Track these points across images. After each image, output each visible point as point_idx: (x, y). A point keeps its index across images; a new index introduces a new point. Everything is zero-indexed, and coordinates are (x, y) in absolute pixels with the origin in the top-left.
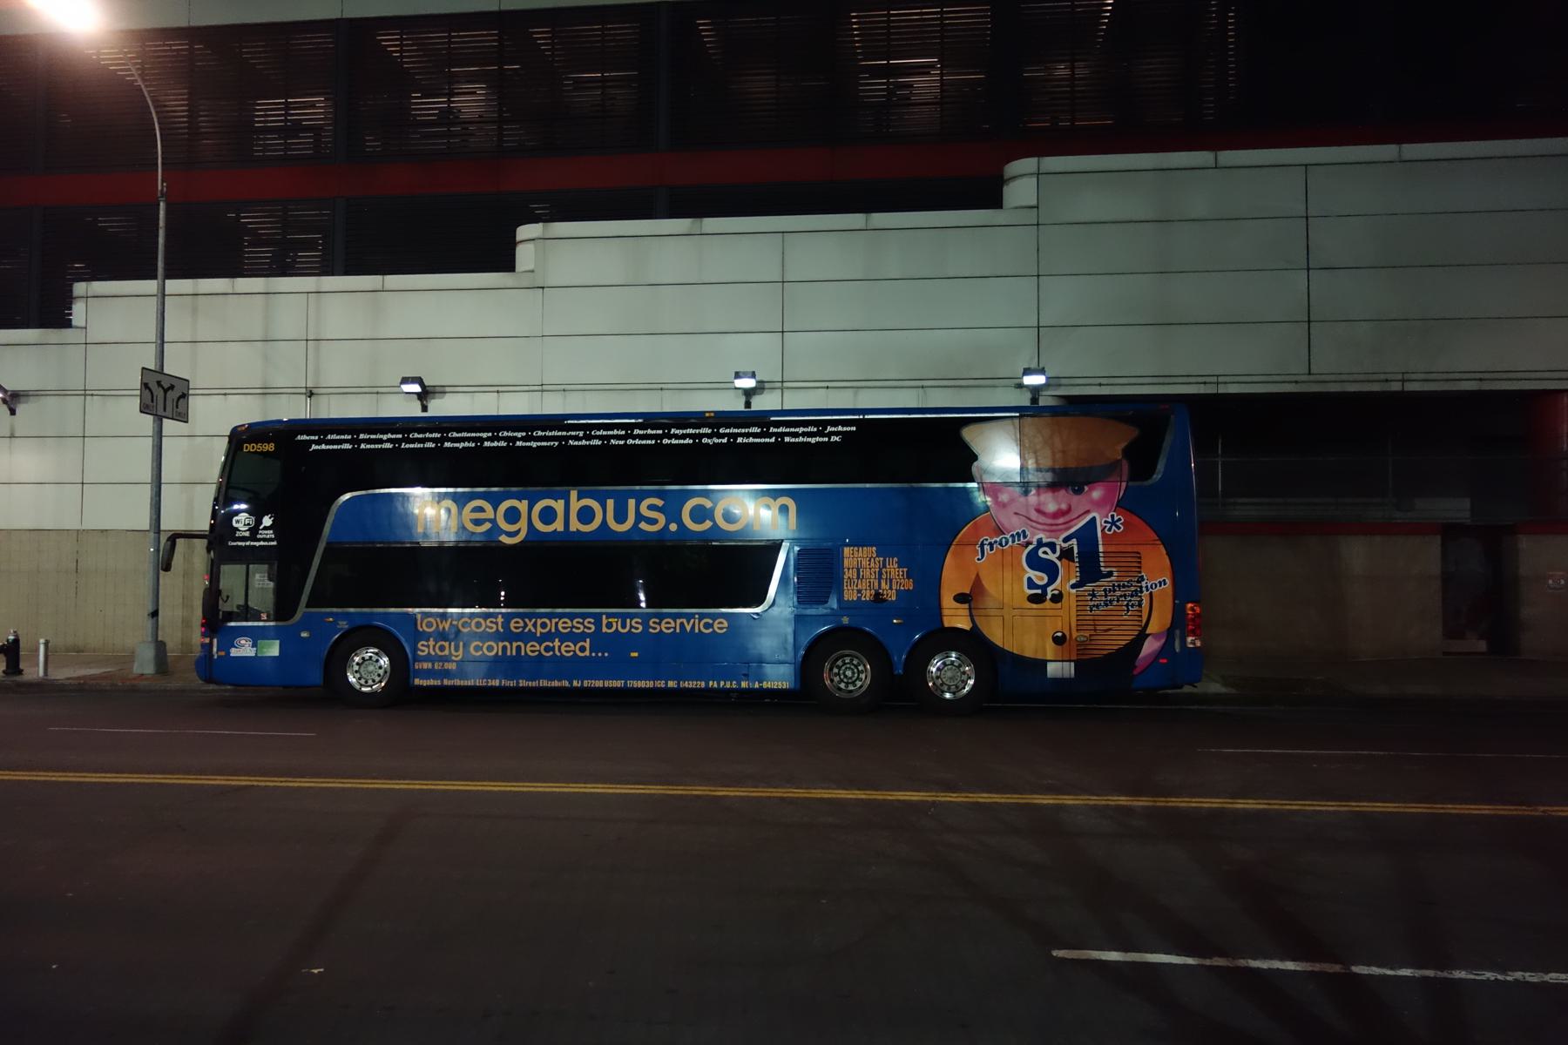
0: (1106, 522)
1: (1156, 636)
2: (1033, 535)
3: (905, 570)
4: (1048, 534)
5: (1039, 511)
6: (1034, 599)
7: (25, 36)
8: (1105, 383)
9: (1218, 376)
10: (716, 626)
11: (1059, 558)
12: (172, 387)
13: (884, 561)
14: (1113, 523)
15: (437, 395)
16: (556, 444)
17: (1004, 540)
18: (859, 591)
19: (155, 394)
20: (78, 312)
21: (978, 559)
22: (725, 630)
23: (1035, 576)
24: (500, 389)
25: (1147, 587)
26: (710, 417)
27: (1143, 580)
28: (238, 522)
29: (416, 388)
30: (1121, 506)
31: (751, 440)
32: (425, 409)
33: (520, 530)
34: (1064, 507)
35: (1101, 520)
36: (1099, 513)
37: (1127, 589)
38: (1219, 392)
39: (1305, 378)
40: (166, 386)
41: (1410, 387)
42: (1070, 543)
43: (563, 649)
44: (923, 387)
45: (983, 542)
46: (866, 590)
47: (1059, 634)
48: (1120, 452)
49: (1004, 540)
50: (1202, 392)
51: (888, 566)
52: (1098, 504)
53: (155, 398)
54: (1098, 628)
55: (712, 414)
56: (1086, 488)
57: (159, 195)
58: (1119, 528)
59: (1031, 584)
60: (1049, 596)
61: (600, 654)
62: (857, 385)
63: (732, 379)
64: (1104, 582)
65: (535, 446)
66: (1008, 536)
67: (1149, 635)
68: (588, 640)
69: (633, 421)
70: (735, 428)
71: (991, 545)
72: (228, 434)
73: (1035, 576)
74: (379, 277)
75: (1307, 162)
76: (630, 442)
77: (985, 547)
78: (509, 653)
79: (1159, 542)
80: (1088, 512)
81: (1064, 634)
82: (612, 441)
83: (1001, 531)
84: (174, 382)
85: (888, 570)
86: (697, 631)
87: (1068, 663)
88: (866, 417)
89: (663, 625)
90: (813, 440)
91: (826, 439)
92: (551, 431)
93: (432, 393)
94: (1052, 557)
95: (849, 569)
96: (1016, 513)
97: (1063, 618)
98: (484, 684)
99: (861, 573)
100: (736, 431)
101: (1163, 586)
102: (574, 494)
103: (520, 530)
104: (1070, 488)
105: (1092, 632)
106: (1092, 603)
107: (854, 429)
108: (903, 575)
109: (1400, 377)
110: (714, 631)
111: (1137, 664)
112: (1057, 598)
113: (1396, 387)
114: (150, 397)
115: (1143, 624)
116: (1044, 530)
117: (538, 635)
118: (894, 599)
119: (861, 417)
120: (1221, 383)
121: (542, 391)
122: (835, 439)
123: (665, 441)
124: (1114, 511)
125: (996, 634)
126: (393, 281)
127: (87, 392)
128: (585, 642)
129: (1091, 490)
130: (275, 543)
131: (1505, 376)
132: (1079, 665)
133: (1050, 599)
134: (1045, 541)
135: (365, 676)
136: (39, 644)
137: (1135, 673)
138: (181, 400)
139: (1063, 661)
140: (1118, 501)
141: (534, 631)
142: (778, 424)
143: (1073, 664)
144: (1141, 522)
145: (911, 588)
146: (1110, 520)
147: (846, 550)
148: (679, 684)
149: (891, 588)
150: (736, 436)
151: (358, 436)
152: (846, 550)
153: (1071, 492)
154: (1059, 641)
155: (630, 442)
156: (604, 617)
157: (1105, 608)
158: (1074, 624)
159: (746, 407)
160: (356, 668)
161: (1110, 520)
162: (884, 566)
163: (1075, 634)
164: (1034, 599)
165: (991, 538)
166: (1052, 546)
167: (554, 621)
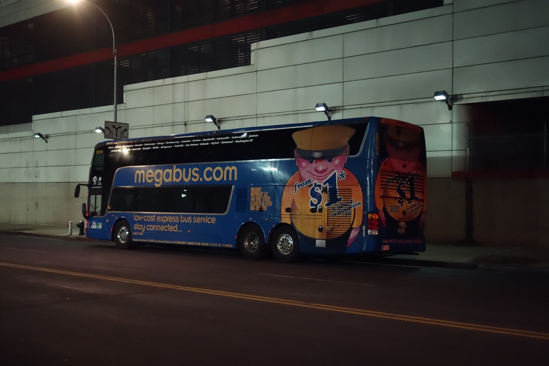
0: (339, 175)
1: (356, 229)
2: (313, 181)
3: (270, 197)
4: (318, 180)
5: (316, 171)
6: (313, 211)
9: (543, 87)
10: (212, 220)
11: (322, 192)
12: (120, 127)
13: (263, 194)
14: (342, 175)
15: (337, 111)
16: (171, 147)
17: (303, 184)
18: (255, 207)
19: (111, 130)
21: (294, 193)
22: (215, 222)
23: (313, 200)
24: (243, 118)
25: (353, 205)
26: (215, 133)
27: (352, 202)
28: (94, 179)
29: (442, 97)
30: (346, 167)
31: (226, 142)
32: (219, 128)
33: (160, 181)
34: (325, 168)
35: (338, 174)
36: (337, 171)
37: (346, 206)
38: (544, 96)
40: (117, 127)
42: (326, 185)
43: (170, 228)
44: (400, 104)
45: (296, 185)
46: (257, 206)
47: (321, 227)
48: (347, 142)
49: (303, 184)
50: (535, 96)
51: (264, 196)
52: (337, 167)
53: (112, 132)
54: (335, 224)
55: (216, 132)
56: (333, 159)
57: (114, 54)
58: (344, 177)
59: (312, 204)
60: (318, 210)
61: (180, 231)
62: (372, 105)
63: (315, 108)
64: (338, 203)
65: (244, 142)
66: (304, 182)
67: (353, 228)
68: (177, 225)
69: (193, 136)
70: (173, 141)
71: (298, 186)
72: (94, 147)
73: (313, 200)
74: (205, 73)
76: (191, 145)
77: (297, 187)
78: (156, 230)
79: (359, 184)
80: (333, 170)
81: (322, 227)
82: (186, 145)
83: (303, 180)
84: (120, 125)
85: (265, 197)
86: (206, 222)
87: (323, 240)
88: (262, 130)
89: (197, 220)
90: (244, 141)
91: (248, 141)
92: (219, 137)
93: (224, 121)
94: (320, 191)
95: (252, 197)
96: (308, 172)
97: (322, 219)
98: (181, 242)
99: (256, 199)
100: (222, 139)
101: (359, 205)
102: (175, 167)
103: (160, 181)
104: (327, 159)
105: (333, 227)
106: (333, 213)
107: (257, 136)
108: (269, 200)
110: (211, 223)
111: (348, 242)
112: (321, 210)
114: (109, 132)
115: (351, 223)
116: (317, 179)
117: (164, 223)
118: (266, 210)
119: (260, 130)
121: (257, 117)
122: (251, 140)
123: (201, 144)
124: (343, 170)
125: (299, 227)
126: (211, 74)
128: (176, 226)
129: (335, 160)
130: (101, 187)
132: (328, 241)
133: (318, 211)
134: (317, 184)
135: (284, 248)
136: (69, 223)
137: (348, 246)
138: (125, 132)
139: (322, 239)
140: (345, 165)
141: (163, 221)
142: (235, 135)
143: (325, 241)
144: (353, 174)
145: (272, 205)
146: (341, 174)
147: (252, 188)
148: (201, 244)
149: (265, 205)
150: (221, 141)
151: (231, 137)
152: (252, 188)
153: (328, 162)
154: (321, 230)
155: (191, 145)
156: (181, 216)
157: (338, 215)
158: (326, 224)
159: (219, 129)
160: (280, 243)
161: (341, 174)
162: (263, 196)
163: (326, 227)
164: (313, 211)
165: (299, 183)
166: (319, 186)
167: (168, 217)
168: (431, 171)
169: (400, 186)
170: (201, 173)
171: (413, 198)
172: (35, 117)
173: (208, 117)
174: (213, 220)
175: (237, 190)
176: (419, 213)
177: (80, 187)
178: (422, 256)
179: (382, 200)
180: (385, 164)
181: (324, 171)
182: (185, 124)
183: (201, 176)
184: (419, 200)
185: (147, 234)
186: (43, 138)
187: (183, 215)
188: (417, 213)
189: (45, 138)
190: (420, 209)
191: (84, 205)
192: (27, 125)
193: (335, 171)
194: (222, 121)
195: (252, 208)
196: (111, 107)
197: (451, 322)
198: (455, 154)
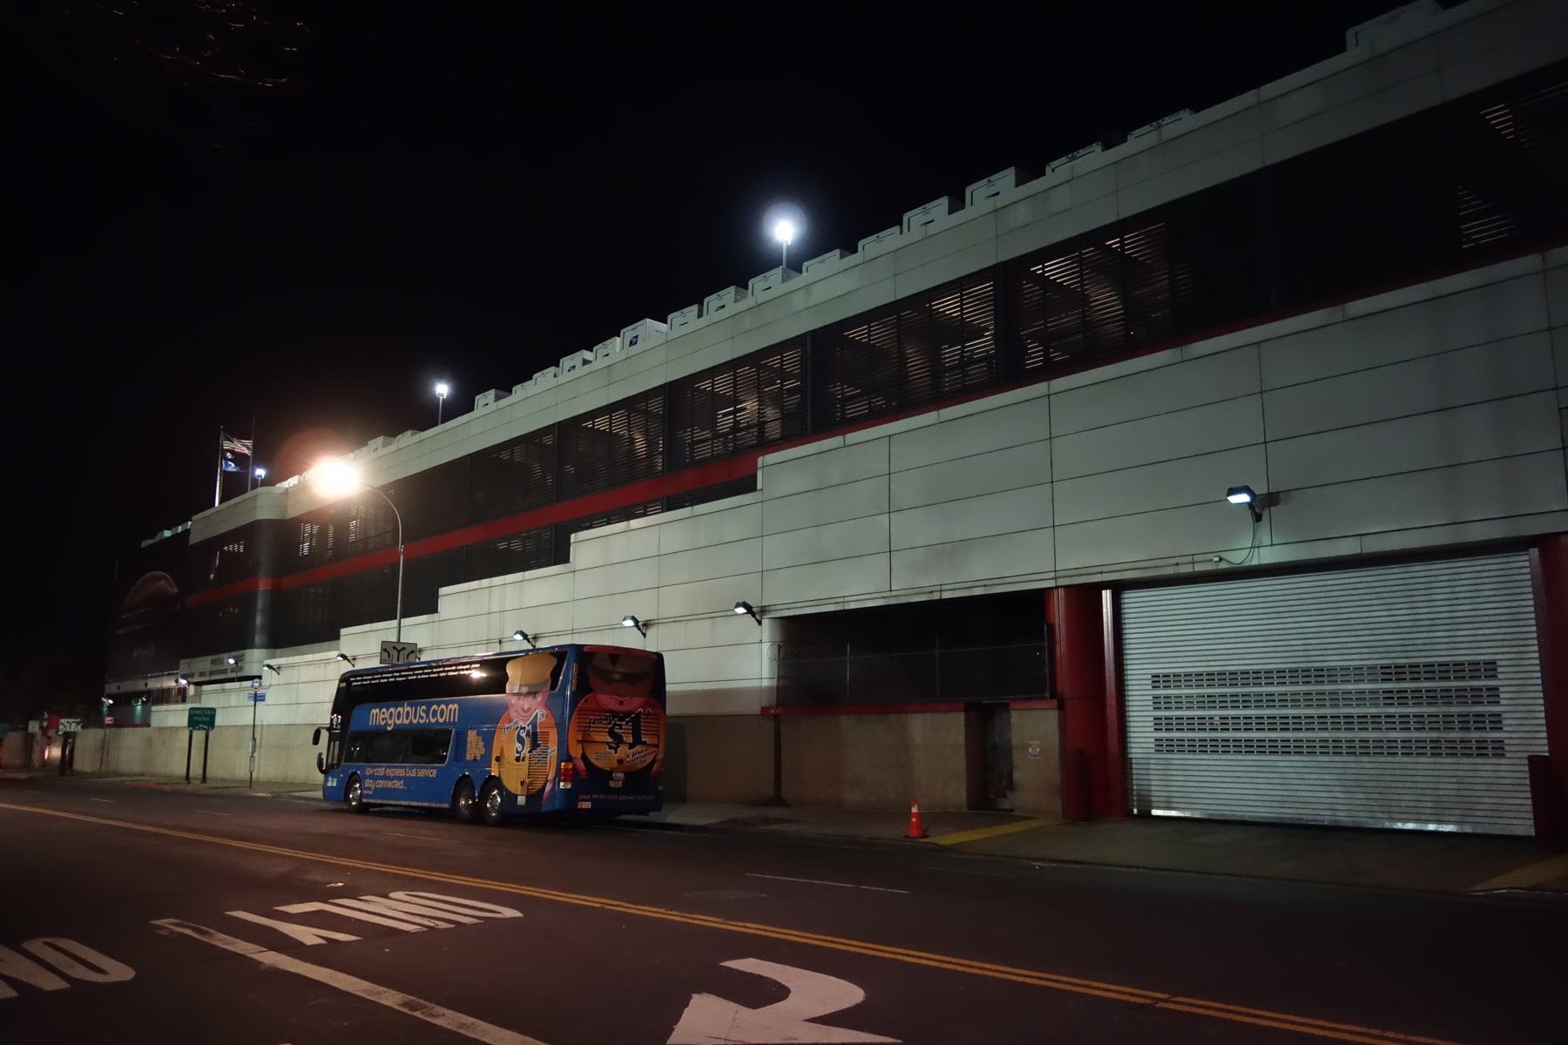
7: (320, 509)
8: (1183, 562)
12: (404, 649)
20: (442, 603)
39: (888, 594)
41: (946, 595)
59: (517, 752)
75: (1257, 341)
109: (938, 588)
113: (936, 596)
120: (1059, 577)
127: (1058, 574)
131: (1000, 581)
164: (518, 759)
166: (524, 728)
168: (671, 709)
169: (613, 728)
170: (427, 712)
171: (637, 741)
172: (344, 631)
173: (738, 605)
174: (435, 772)
175: (458, 734)
176: (648, 762)
177: (319, 732)
178: (653, 816)
179: (580, 746)
180: (586, 701)
181: (529, 710)
182: (500, 642)
183: (428, 717)
184: (650, 744)
185: (379, 792)
186: (754, 615)
187: (409, 767)
188: (645, 761)
189: (531, 640)
190: (652, 756)
191: (320, 754)
192: (336, 642)
193: (537, 711)
194: (651, 624)
195: (468, 758)
196: (394, 623)
197: (494, 883)
198: (765, 683)
